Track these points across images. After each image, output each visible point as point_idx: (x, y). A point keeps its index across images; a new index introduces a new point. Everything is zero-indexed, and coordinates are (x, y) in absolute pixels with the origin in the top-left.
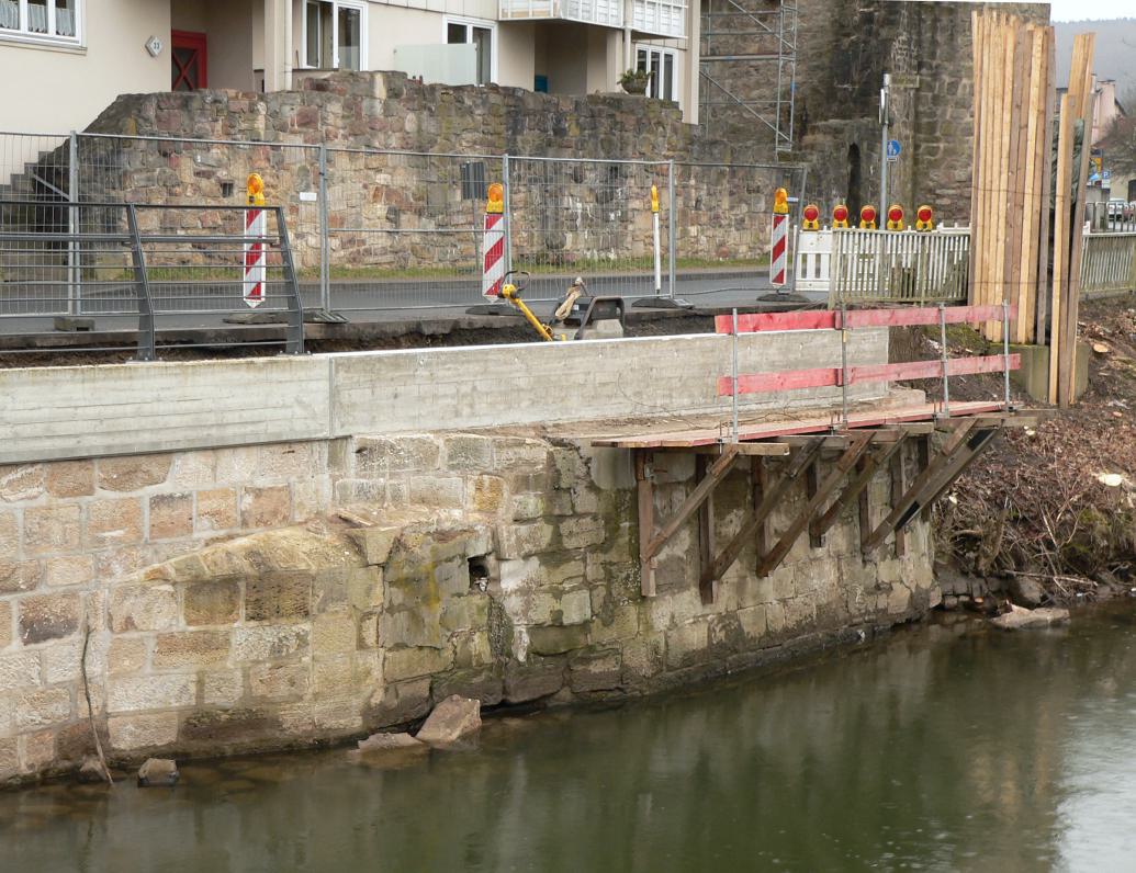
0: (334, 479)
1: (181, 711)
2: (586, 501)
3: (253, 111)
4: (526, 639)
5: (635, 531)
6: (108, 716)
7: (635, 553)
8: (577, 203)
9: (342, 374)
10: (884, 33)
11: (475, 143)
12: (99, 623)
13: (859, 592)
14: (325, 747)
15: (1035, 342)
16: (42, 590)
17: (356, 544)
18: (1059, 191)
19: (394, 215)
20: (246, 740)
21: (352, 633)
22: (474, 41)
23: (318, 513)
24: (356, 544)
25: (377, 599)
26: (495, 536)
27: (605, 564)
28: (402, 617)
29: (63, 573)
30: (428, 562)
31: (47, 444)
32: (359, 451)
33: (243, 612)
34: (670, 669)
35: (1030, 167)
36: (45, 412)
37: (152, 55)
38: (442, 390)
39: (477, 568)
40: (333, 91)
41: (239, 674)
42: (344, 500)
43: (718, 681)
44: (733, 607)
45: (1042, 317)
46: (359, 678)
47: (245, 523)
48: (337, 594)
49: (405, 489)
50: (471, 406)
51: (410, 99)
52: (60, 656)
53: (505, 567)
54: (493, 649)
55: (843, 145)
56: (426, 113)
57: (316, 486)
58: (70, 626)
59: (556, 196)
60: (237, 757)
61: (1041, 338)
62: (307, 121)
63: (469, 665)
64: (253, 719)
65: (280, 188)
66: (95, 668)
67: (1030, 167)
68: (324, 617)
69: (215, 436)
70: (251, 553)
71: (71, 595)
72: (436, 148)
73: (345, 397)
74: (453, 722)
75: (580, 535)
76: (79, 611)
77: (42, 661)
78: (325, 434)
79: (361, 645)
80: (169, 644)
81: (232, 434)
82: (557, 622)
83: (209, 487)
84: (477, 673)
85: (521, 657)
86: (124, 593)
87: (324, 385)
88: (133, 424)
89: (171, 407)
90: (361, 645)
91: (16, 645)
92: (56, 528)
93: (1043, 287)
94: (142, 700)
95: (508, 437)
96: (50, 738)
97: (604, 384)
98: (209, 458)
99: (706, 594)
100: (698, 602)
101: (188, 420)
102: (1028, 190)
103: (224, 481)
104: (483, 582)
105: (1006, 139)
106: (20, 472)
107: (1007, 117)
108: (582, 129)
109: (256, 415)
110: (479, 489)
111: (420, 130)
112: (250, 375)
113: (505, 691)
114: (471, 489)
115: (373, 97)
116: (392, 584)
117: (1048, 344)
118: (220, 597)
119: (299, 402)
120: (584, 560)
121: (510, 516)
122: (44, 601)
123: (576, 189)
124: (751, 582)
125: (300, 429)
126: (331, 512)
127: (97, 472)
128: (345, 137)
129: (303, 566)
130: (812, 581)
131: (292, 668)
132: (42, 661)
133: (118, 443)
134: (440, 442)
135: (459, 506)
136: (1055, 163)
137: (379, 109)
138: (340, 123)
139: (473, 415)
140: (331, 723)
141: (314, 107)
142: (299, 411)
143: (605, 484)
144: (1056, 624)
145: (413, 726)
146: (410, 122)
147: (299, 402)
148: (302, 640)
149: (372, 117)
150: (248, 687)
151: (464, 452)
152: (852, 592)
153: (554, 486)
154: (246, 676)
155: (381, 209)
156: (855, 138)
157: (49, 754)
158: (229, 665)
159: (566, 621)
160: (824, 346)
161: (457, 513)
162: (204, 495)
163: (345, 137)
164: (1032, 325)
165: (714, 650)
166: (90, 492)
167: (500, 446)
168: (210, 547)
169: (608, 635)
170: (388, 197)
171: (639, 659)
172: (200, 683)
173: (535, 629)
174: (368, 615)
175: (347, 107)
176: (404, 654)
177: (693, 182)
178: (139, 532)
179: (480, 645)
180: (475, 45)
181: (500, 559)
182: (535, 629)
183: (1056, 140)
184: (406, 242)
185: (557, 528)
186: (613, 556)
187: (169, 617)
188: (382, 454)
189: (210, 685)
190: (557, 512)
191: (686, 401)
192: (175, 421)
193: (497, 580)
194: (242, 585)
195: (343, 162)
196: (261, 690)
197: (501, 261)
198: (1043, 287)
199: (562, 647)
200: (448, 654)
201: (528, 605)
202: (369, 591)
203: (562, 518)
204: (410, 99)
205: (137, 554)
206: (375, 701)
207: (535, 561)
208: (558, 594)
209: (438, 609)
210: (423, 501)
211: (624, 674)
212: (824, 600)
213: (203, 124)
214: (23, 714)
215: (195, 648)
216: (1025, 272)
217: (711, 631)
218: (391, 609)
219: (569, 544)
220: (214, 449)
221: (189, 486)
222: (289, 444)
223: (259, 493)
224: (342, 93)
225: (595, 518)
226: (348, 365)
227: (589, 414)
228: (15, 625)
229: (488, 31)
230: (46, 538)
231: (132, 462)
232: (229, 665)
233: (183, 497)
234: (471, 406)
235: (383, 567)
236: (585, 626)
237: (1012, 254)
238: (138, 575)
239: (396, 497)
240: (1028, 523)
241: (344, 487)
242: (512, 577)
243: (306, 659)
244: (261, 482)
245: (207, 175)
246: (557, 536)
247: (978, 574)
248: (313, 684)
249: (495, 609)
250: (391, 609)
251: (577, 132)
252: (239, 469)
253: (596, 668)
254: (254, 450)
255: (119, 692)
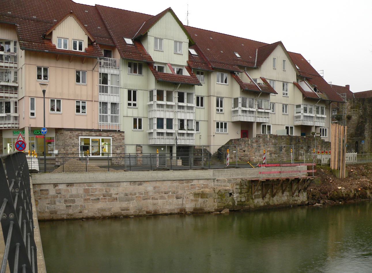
0: (214, 184)
1: (193, 208)
2: (245, 187)
3: (248, 140)
4: (237, 203)
5: (252, 191)
6: (185, 208)
7: (252, 193)
8: (302, 152)
9: (214, 172)
10: (364, 124)
11: (284, 143)
12: (185, 198)
13: (291, 201)
14: (209, 213)
15: (338, 169)
16: (178, 194)
17: (214, 191)
18: (341, 148)
19: (271, 154)
20: (201, 211)
21: (213, 200)
22: (286, 129)
23: (212, 187)
24: (214, 191)
25: (217, 197)
26: (233, 190)
27: (247, 194)
28: (220, 199)
29: (180, 192)
30: (224, 193)
31: (178, 178)
32: (217, 180)
33: (200, 197)
34: (257, 208)
35: (337, 145)
36: (178, 175)
37: (238, 134)
38: (228, 174)
39: (231, 194)
40: (261, 137)
41: (200, 204)
42: (215, 186)
43: (267, 209)
44: (268, 201)
45: (339, 166)
46: (214, 206)
47: (202, 188)
48: (211, 196)
49: (222, 185)
50: (232, 175)
51: (273, 138)
52: (180, 201)
53: (234, 194)
54: (232, 204)
55: (354, 141)
56: (276, 140)
57: (211, 184)
58: (181, 198)
59: (298, 151)
60: (200, 213)
61: (339, 169)
62: (257, 142)
63: (229, 205)
64: (201, 209)
65: (253, 151)
66: (184, 202)
67: (337, 145)
68: (209, 198)
69: (198, 178)
70: (202, 191)
71: (181, 194)
72: (278, 144)
73: (215, 174)
74: (226, 211)
75: (244, 191)
76: (182, 196)
77: (178, 201)
78: (212, 178)
79: (214, 202)
80: (192, 200)
81: (200, 178)
82: (241, 201)
83: (198, 184)
84: (230, 206)
85: (236, 205)
86: (187, 195)
87: (212, 173)
88: (188, 176)
89: (193, 175)
90: (214, 202)
91: (175, 199)
92: (180, 187)
93: (339, 162)
94: (189, 206)
95: (236, 179)
96: (179, 209)
97: (252, 173)
98: (198, 180)
99: (263, 199)
100: (262, 200)
101: (195, 176)
102: (337, 148)
103: (199, 183)
104: (232, 196)
105: (334, 141)
106: (175, 181)
107: (334, 138)
108: (303, 141)
109: (203, 176)
110: (231, 185)
111: (275, 142)
112: (203, 171)
113: (234, 209)
114: (230, 185)
115: (267, 138)
116: (218, 195)
117: (340, 170)
118: (197, 196)
119: (209, 175)
120: (245, 194)
121: (235, 188)
122: (178, 195)
123: (302, 150)
124: (271, 198)
125: (209, 178)
126: (213, 187)
127: (184, 181)
128: (263, 144)
129: (207, 193)
130: (282, 198)
131: (206, 204)
132: (178, 201)
133: (186, 178)
134: (227, 179)
135: (229, 187)
136: (340, 144)
137: (268, 139)
138: (262, 142)
139: (233, 177)
140: (210, 210)
141: (258, 140)
142: (209, 176)
143: (248, 185)
144: (320, 206)
145: (220, 212)
146: (273, 141)
147: (209, 175)
148: (207, 201)
149: (267, 141)
150: (201, 206)
151: (229, 181)
152: (290, 201)
153: (241, 185)
154: (200, 204)
155: (268, 153)
156: (357, 140)
157: (179, 211)
158: (199, 203)
159: (242, 201)
160: (288, 169)
161: (228, 188)
162: (197, 185)
163: (263, 144)
164: (337, 167)
165: (264, 206)
166: (183, 184)
167: (234, 180)
168: (197, 190)
169: (248, 203)
170: (270, 152)
171: (252, 206)
172: (195, 205)
173: (238, 202)
174: (215, 199)
175: (263, 139)
176: (220, 203)
177: (323, 148)
178: (189, 188)
179: (231, 203)
180: (286, 130)
181: (234, 193)
182: (238, 202)
183: (340, 141)
184: (273, 158)
185: (241, 190)
186: (248, 193)
187: (192, 197)
188: (220, 181)
189: (196, 205)
190: (241, 188)
191: (265, 176)
192: (193, 176)
193: (233, 196)
194: (200, 194)
195: (262, 147)
196: (202, 206)
197: (265, 160)
198: (339, 162)
199: (241, 204)
200: (226, 204)
201: (237, 199)
202: (215, 196)
203: (242, 189)
204: (273, 138)
205: (189, 190)
206: (217, 208)
207: (238, 194)
208: (241, 198)
209: (225, 199)
210: (224, 186)
211: (250, 208)
212: (284, 201)
213: (241, 143)
214: (176, 206)
215: (195, 201)
216: (337, 160)
217: (264, 203)
218: (218, 198)
219: (243, 192)
220: (198, 179)
221: (195, 183)
222: (208, 179)
223: (204, 185)
224: (262, 137)
225: (246, 189)
226: (215, 171)
227: (250, 177)
228: (175, 197)
229: (293, 127)
230: (178, 188)
231: (188, 181)
232: (199, 203)
233: (194, 185)
234: (232, 175)
235: (217, 193)
236: (245, 202)
237: (335, 157)
238: (189, 193)
239: (221, 186)
240: (326, 193)
241: (215, 185)
242: (235, 195)
243: (207, 203)
244: (204, 184)
245: (241, 150)
246: (241, 191)
247: (315, 200)
248: (208, 206)
249: (233, 199)
250: (218, 198)
251: (302, 141)
252: (201, 182)
253: (246, 207)
254: (203, 180)
255: (187, 205)
